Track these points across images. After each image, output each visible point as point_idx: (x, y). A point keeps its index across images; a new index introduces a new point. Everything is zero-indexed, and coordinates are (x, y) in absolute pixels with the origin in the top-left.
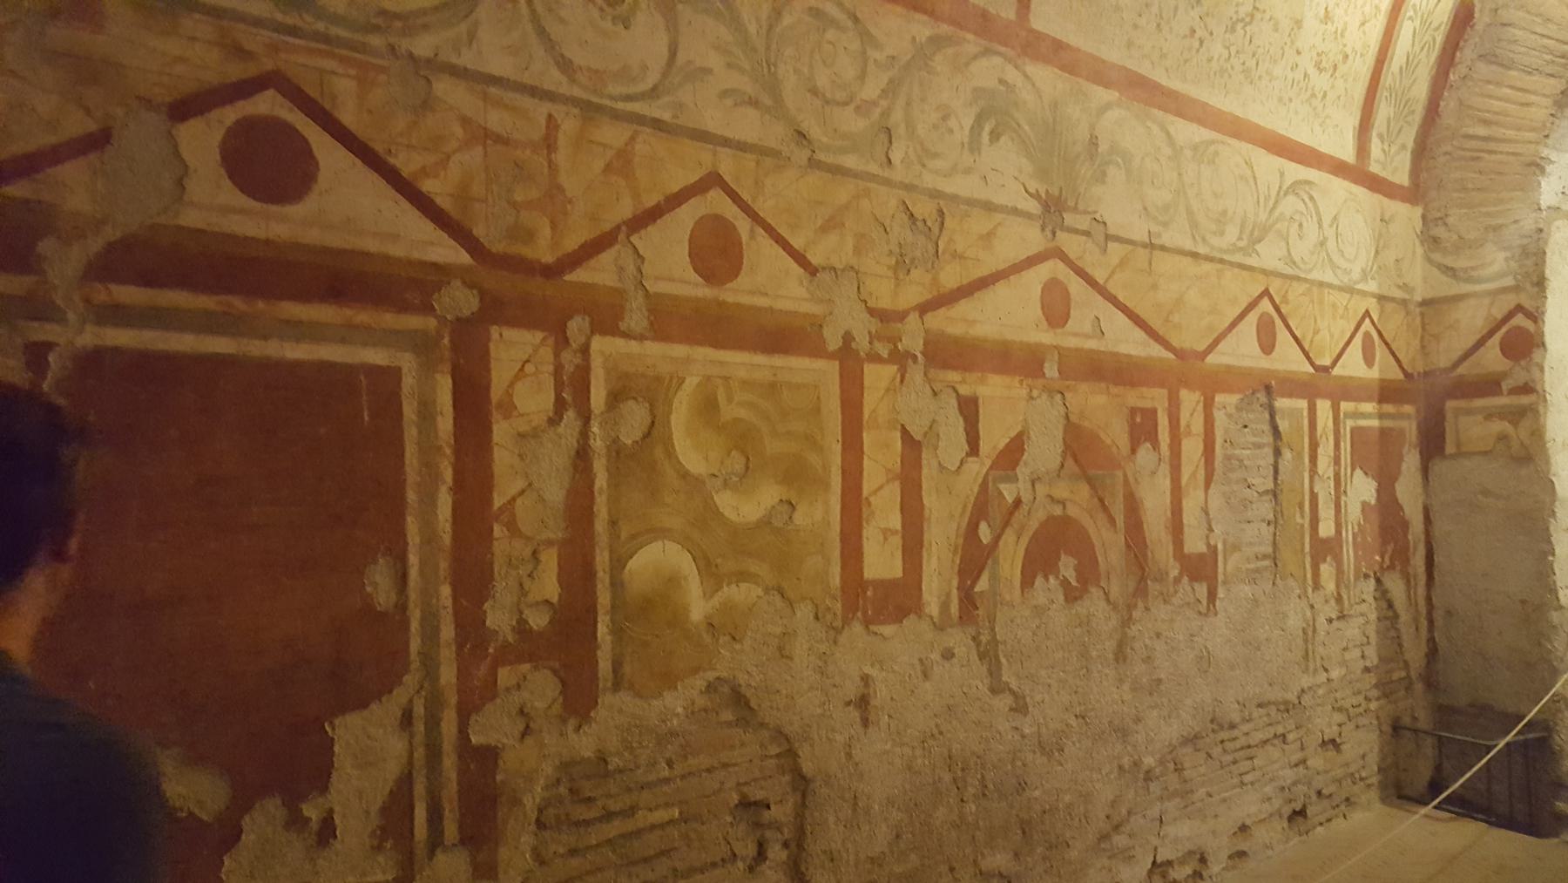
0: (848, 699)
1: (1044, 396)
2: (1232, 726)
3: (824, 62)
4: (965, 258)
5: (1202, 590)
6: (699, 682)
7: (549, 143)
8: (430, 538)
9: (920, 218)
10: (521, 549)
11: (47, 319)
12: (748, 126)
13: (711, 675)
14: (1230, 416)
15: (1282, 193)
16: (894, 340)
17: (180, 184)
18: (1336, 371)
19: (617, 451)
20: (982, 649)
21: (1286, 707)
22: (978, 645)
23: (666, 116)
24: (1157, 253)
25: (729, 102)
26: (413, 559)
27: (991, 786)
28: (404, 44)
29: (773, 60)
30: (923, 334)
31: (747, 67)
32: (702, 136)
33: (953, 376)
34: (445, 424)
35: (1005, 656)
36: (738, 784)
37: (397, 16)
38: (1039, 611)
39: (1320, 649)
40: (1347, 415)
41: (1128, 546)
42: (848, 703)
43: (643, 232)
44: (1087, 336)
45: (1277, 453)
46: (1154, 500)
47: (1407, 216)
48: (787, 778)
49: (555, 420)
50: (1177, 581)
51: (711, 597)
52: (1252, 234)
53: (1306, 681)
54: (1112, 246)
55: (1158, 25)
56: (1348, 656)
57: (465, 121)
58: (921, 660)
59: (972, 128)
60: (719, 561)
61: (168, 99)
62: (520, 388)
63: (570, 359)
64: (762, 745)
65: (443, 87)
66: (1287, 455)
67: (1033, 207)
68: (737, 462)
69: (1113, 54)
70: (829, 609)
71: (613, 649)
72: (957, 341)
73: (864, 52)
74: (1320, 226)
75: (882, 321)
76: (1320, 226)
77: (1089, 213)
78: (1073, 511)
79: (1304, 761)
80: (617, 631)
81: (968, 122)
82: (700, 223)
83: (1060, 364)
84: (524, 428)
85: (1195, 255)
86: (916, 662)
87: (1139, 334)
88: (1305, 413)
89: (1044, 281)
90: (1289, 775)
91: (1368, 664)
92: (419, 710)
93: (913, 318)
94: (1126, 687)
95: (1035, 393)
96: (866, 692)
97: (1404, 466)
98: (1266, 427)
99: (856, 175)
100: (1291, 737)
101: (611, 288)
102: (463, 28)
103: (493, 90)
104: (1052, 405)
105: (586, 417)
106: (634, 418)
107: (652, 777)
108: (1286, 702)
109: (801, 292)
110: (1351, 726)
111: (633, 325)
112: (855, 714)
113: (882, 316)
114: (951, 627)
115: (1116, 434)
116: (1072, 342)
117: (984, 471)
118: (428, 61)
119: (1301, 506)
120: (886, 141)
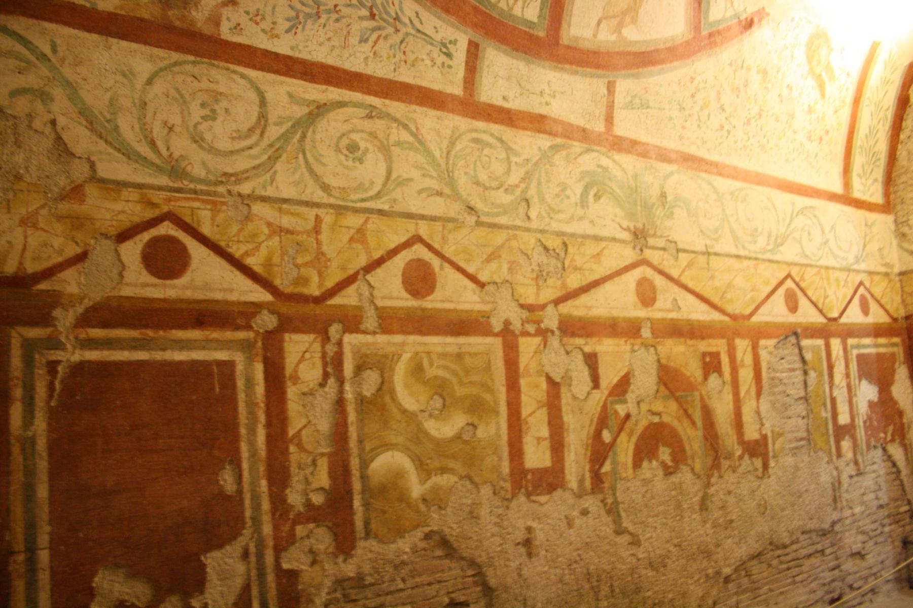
0: (517, 541)
1: (643, 350)
2: (785, 547)
3: (483, 167)
4: (584, 270)
5: (758, 463)
6: (419, 533)
7: (317, 230)
8: (254, 455)
9: (551, 248)
10: (306, 459)
11: (56, 349)
12: (436, 207)
13: (427, 529)
14: (771, 353)
15: (794, 215)
16: (538, 322)
17: (121, 275)
18: (843, 320)
19: (361, 400)
20: (608, 508)
21: (824, 533)
22: (605, 505)
23: (386, 207)
24: (712, 258)
25: (424, 195)
26: (245, 465)
27: (617, 590)
28: (236, 189)
29: (451, 169)
30: (557, 317)
31: (434, 174)
32: (409, 216)
33: (579, 341)
34: (260, 389)
35: (624, 511)
36: (449, 593)
37: (232, 175)
38: (646, 482)
39: (845, 495)
40: (853, 347)
41: (706, 439)
42: (518, 544)
43: (373, 273)
44: (669, 311)
45: (805, 373)
46: (722, 409)
47: (883, 222)
48: (479, 589)
49: (322, 385)
50: (741, 458)
51: (424, 483)
52: (776, 239)
53: (835, 516)
54: (681, 255)
55: (699, 126)
56: (866, 498)
57: (269, 224)
58: (566, 517)
59: (582, 194)
60: (428, 461)
61: (115, 233)
62: (301, 366)
63: (331, 349)
64: (462, 570)
65: (258, 208)
66: (812, 375)
67: (626, 236)
68: (437, 402)
69: (671, 144)
70: (502, 488)
71: (364, 514)
72: (581, 319)
73: (508, 159)
74: (823, 232)
75: (529, 311)
76: (823, 232)
77: (664, 237)
78: (666, 419)
79: (837, 567)
80: (366, 505)
81: (579, 190)
82: (409, 264)
83: (652, 328)
84: (305, 390)
85: (738, 257)
86: (563, 517)
87: (704, 307)
88: (823, 348)
89: (637, 279)
90: (828, 576)
91: (881, 502)
92: (252, 549)
93: (550, 309)
94: (708, 525)
95: (636, 348)
96: (529, 536)
97: (897, 377)
98: (797, 358)
99: (507, 228)
100: (828, 551)
101: (354, 306)
102: (268, 176)
103: (284, 206)
104: (648, 354)
105: (341, 381)
106: (371, 379)
107: (392, 588)
108: (823, 530)
109: (476, 298)
110: (871, 543)
111: (368, 326)
112: (522, 550)
113: (530, 308)
114: (586, 495)
115: (694, 370)
116: (659, 315)
117: (604, 398)
118: (249, 196)
119: (825, 405)
120: (526, 206)
